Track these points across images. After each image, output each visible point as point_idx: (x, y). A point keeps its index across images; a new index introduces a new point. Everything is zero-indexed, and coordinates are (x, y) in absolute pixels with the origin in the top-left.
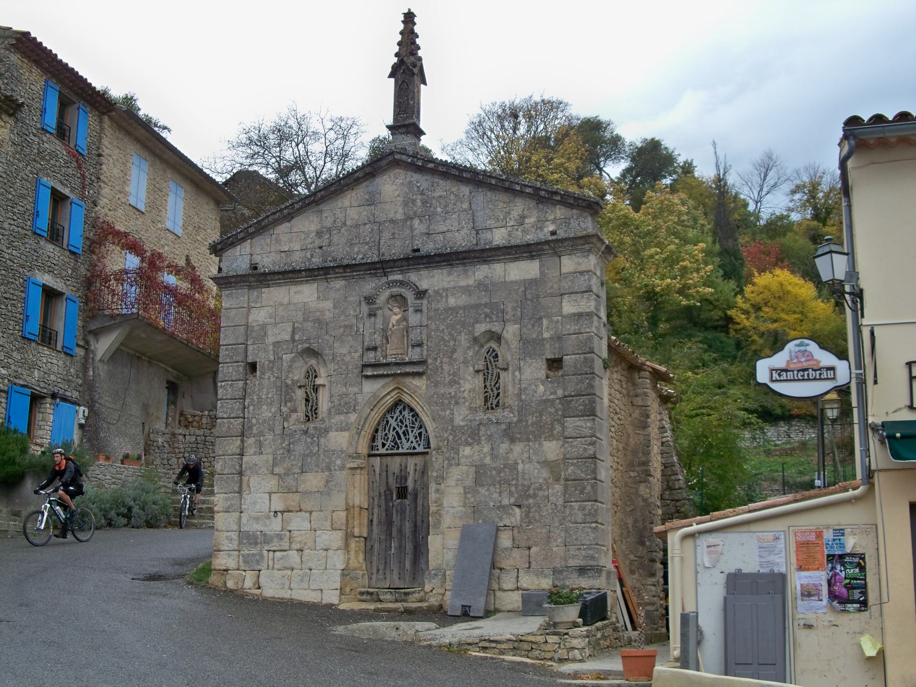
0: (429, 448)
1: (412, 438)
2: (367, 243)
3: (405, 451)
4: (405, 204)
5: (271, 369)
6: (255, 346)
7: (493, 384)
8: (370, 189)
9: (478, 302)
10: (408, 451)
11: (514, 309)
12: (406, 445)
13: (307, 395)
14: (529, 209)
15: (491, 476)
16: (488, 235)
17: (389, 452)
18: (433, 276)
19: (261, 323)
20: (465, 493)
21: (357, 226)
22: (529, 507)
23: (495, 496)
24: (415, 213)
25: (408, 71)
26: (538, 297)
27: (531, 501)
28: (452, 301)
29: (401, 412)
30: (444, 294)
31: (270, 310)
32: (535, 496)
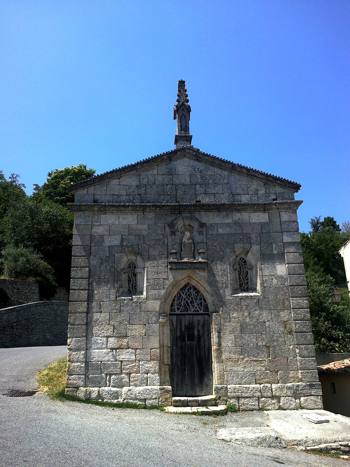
0: (208, 311)
1: (196, 305)
2: (169, 195)
3: (192, 313)
4: (191, 176)
5: (107, 261)
6: (96, 247)
7: (244, 277)
8: (169, 166)
9: (235, 232)
10: (194, 313)
11: (256, 237)
12: (193, 309)
13: (129, 278)
14: (260, 186)
15: (250, 329)
16: (239, 197)
17: (182, 313)
18: (209, 216)
19: (100, 234)
20: (235, 338)
21: (162, 185)
22: (274, 347)
23: (254, 340)
24: (197, 181)
25: (182, 111)
26: (269, 232)
27: (275, 344)
28: (220, 231)
29: (188, 290)
30: (216, 226)
31: (106, 227)
32: (277, 341)
